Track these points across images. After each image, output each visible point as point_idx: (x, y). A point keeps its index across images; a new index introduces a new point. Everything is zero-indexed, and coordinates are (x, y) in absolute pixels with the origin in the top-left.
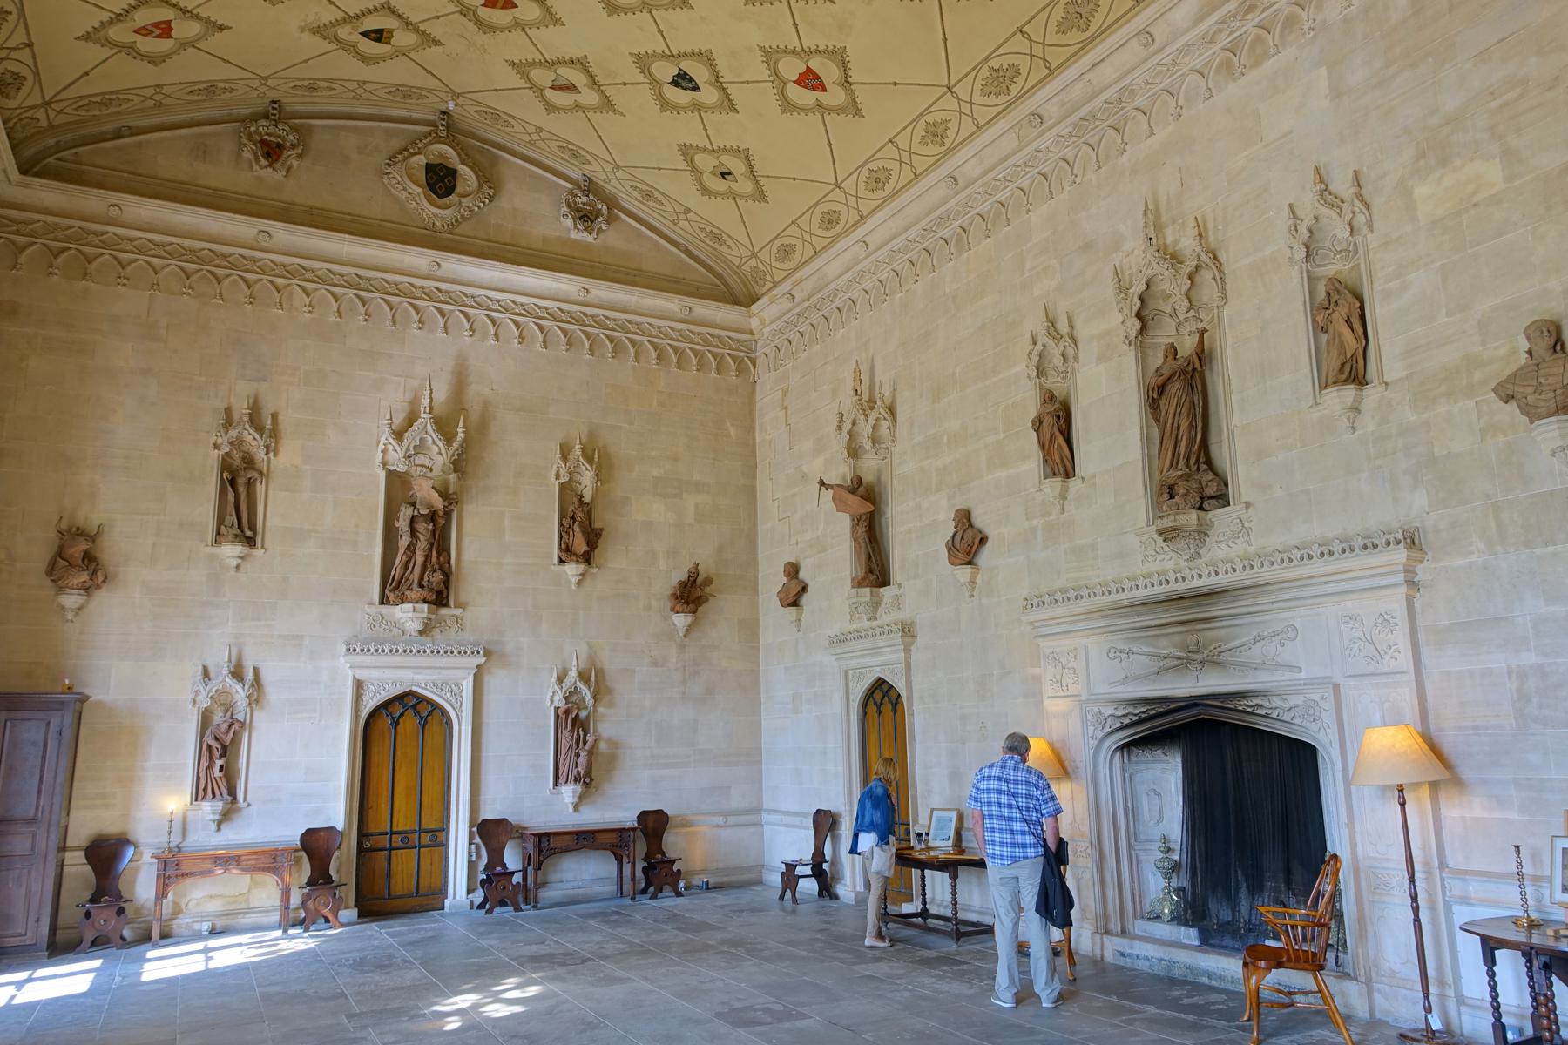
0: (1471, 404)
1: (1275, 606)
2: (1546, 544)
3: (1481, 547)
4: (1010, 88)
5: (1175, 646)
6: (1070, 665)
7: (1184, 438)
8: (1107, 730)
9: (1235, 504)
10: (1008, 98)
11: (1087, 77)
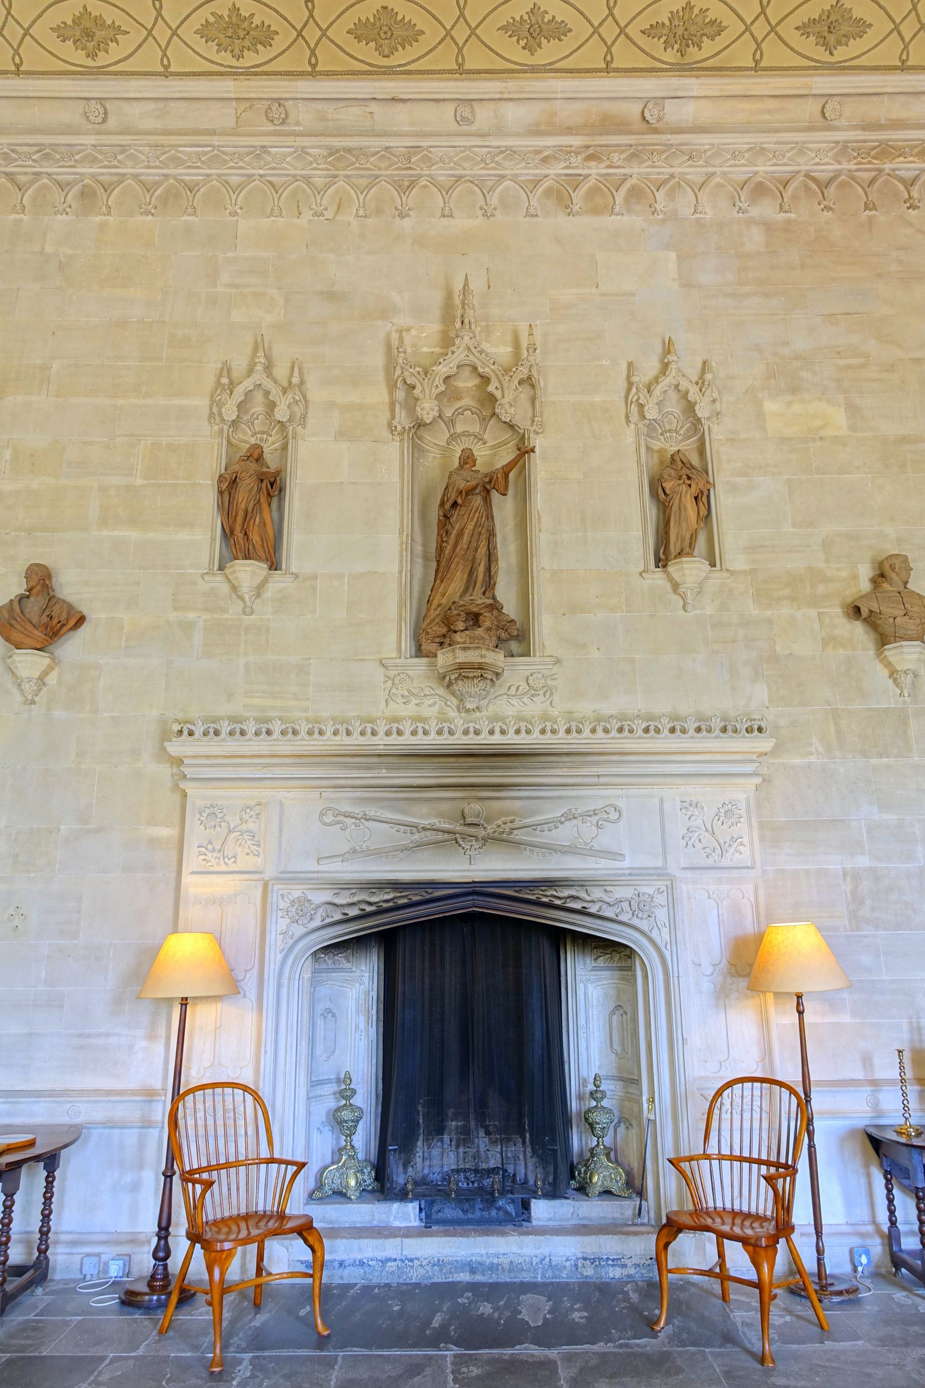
0: (813, 613)
1: (602, 780)
2: (881, 755)
3: (821, 749)
4: (246, 52)
5: (441, 815)
6: (244, 827)
8: (317, 923)
9: (534, 656)
10: (234, 63)
11: (374, 107)
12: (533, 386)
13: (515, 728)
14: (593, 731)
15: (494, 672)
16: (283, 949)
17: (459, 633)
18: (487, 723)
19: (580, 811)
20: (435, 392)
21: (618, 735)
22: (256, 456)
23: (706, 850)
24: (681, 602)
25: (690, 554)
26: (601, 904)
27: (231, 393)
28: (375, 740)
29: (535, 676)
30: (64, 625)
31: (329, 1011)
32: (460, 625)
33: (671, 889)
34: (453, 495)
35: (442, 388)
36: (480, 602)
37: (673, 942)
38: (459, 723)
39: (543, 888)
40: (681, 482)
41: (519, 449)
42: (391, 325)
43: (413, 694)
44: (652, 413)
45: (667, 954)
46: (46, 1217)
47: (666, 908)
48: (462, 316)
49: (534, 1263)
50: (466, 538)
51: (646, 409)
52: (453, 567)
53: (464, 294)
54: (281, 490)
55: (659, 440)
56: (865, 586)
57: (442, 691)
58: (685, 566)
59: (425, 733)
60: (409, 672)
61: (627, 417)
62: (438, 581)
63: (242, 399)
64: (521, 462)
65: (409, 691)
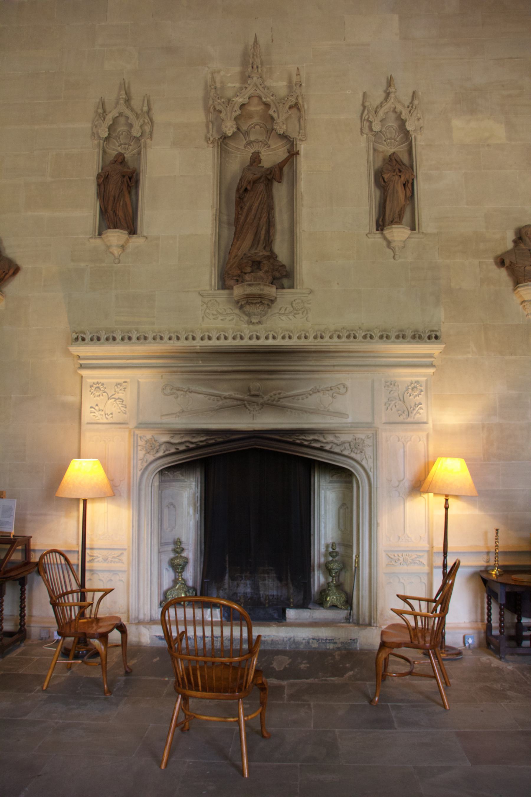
2: (511, 354)
6: (116, 396)
7: (264, 228)
8: (161, 454)
9: (297, 288)
12: (299, 109)
13: (282, 335)
14: (331, 337)
15: (270, 300)
16: (141, 469)
17: (247, 274)
18: (264, 332)
19: (322, 387)
20: (234, 115)
21: (346, 340)
22: (120, 160)
23: (399, 412)
24: (392, 254)
25: (399, 222)
26: (333, 444)
27: (104, 119)
28: (194, 343)
29: (297, 301)
30: (6, 274)
31: (172, 504)
32: (248, 269)
33: (375, 435)
34: (245, 185)
35: (239, 112)
36: (261, 254)
37: (375, 467)
38: (247, 333)
39: (297, 435)
40: (394, 174)
41: (289, 152)
42: (207, 69)
43: (220, 313)
44: (376, 127)
45: (371, 474)
46: (22, 609)
47: (371, 448)
48: (252, 63)
49: (285, 641)
50: (253, 212)
51: (373, 124)
52: (245, 231)
53: (254, 48)
54: (137, 182)
55: (383, 145)
56: (510, 245)
57: (237, 311)
58: (394, 230)
59: (226, 338)
60: (217, 299)
61: (361, 129)
62: (235, 240)
63: (111, 122)
64: (291, 160)
65: (217, 311)
